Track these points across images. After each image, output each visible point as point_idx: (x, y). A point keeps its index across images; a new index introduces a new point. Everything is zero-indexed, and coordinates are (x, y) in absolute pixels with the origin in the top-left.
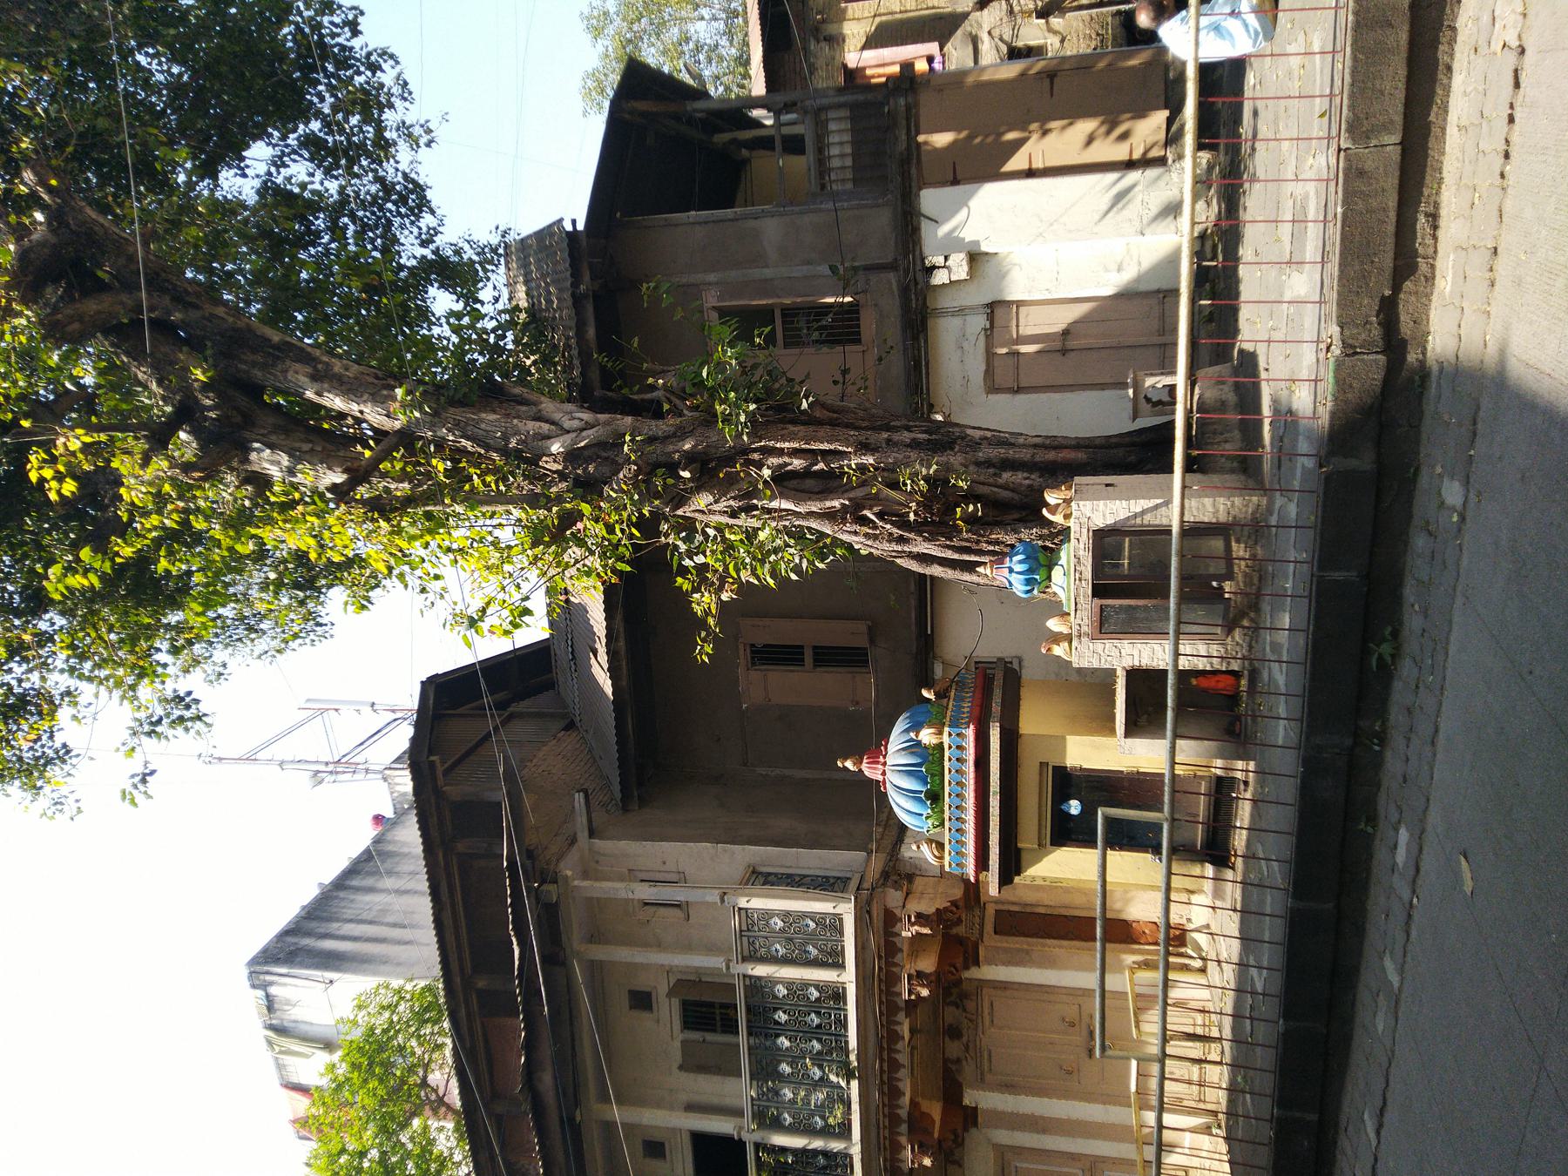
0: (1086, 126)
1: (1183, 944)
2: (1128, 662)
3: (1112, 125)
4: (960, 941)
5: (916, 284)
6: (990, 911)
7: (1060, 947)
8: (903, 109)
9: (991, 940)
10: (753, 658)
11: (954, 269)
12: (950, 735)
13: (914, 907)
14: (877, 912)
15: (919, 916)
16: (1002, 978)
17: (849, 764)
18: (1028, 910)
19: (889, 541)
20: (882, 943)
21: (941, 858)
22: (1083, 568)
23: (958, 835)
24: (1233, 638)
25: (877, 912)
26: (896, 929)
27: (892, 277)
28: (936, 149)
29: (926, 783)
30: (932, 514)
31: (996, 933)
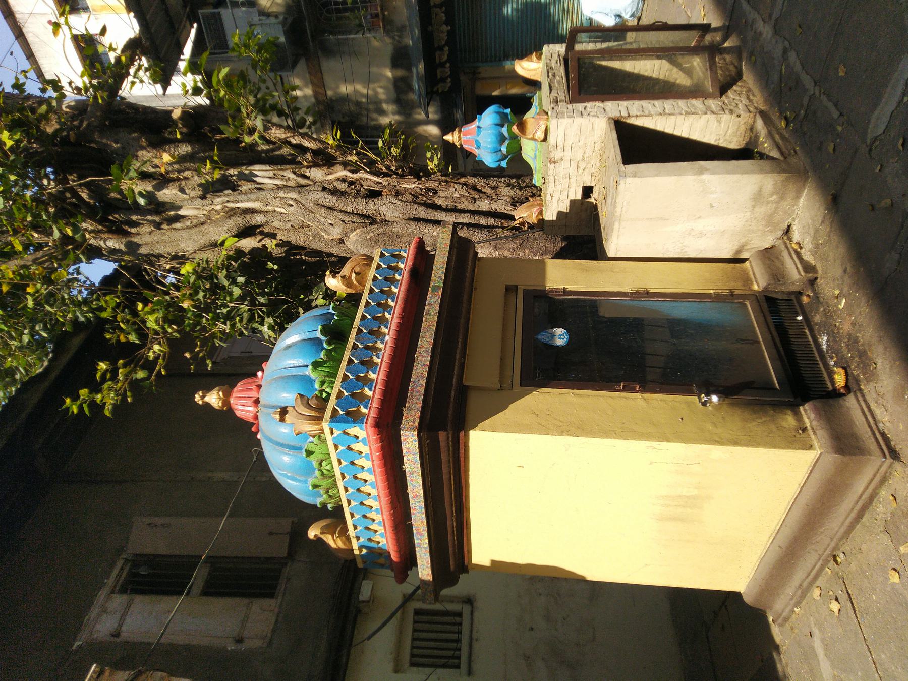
17: (214, 399)
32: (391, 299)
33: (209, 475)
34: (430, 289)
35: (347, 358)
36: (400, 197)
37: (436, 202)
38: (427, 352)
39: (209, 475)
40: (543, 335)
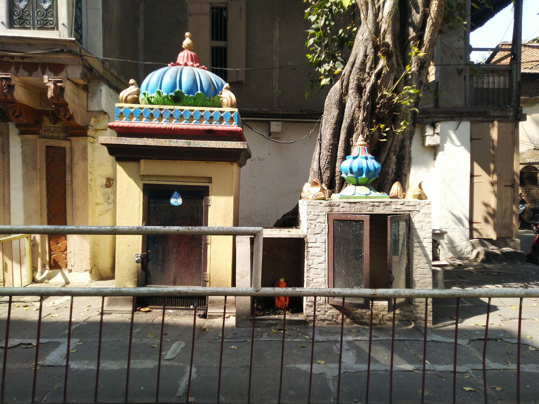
0: (493, 202)
1: (51, 268)
2: (310, 239)
3: (493, 216)
4: (39, 122)
5: (427, 118)
6: (65, 144)
7: (41, 190)
8: (508, 115)
9: (41, 144)
10: (217, 8)
11: (433, 138)
12: (232, 112)
13: (68, 87)
14: (62, 58)
15: (62, 89)
16: (12, 150)
17: (187, 42)
18: (68, 169)
19: (358, 79)
20: (35, 61)
21: (126, 101)
22: (382, 207)
23: (148, 115)
24: (330, 308)
25: (62, 58)
26: (47, 71)
27: (432, 105)
28: (489, 129)
29: (189, 92)
30: (380, 108)
31: (47, 147)
32: (196, 122)
33: (277, 28)
34: (189, 141)
35: (163, 108)
36: (357, 109)
37: (355, 133)
38: (144, 143)
39: (277, 28)
40: (177, 194)
